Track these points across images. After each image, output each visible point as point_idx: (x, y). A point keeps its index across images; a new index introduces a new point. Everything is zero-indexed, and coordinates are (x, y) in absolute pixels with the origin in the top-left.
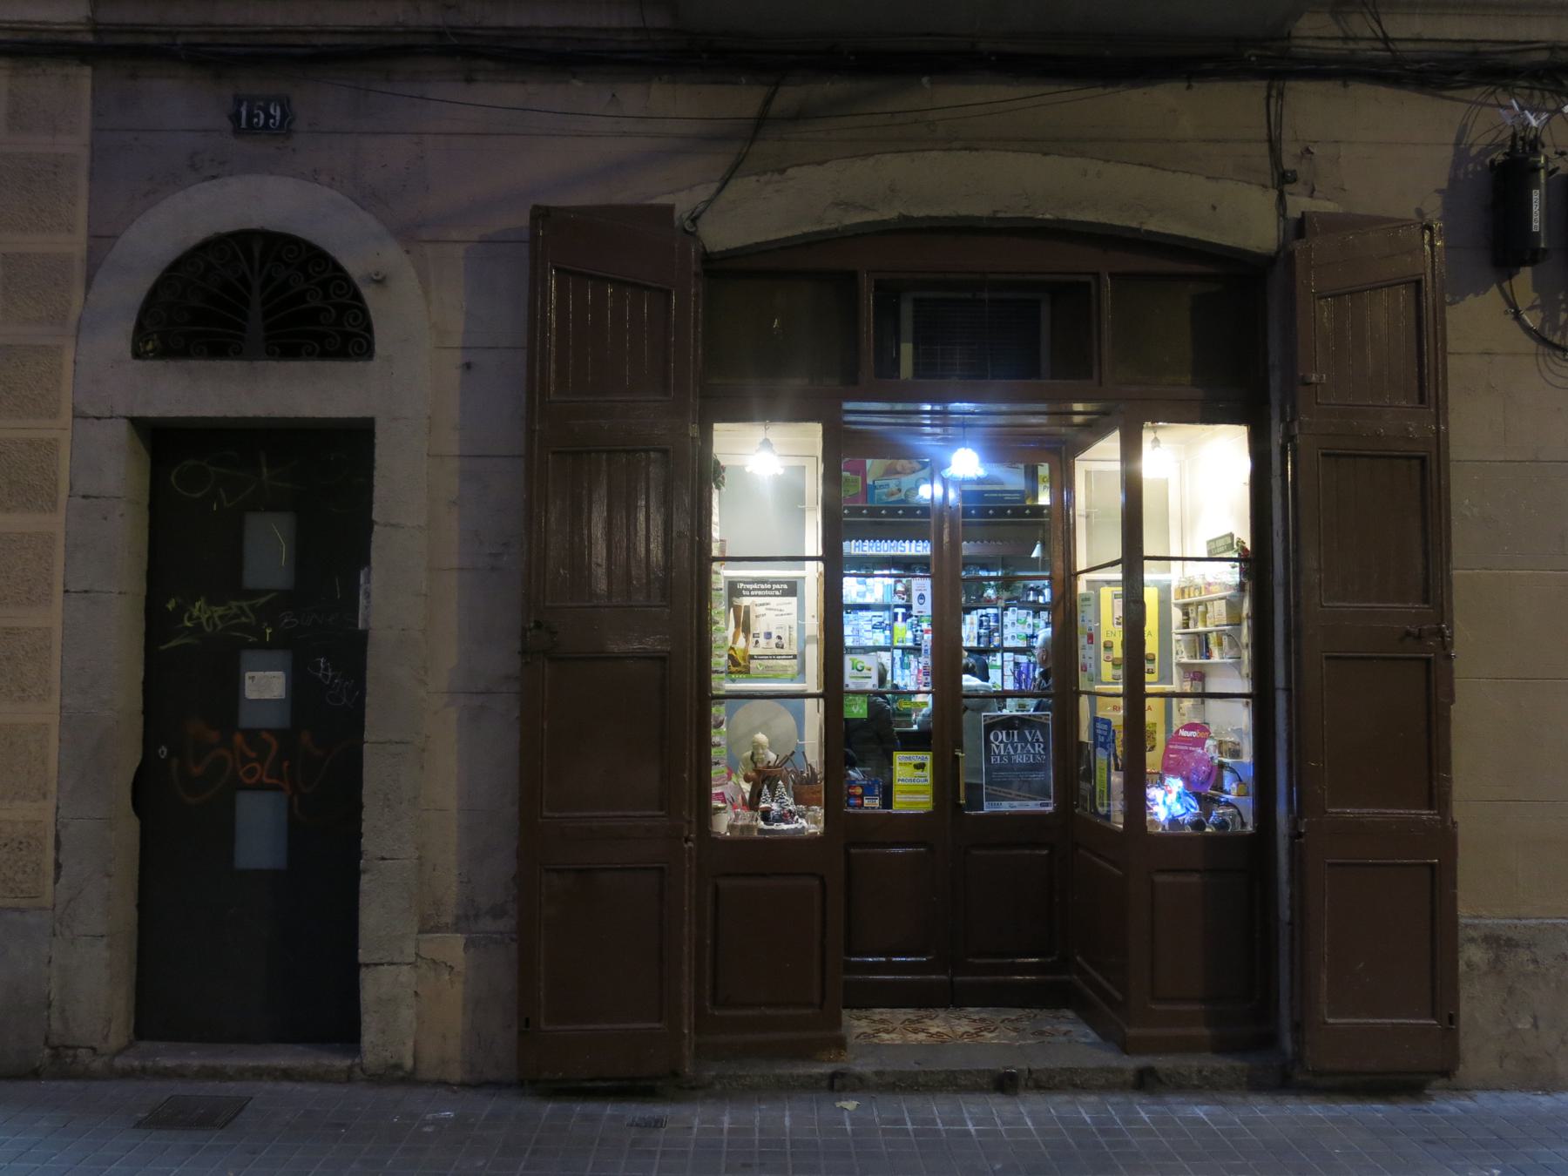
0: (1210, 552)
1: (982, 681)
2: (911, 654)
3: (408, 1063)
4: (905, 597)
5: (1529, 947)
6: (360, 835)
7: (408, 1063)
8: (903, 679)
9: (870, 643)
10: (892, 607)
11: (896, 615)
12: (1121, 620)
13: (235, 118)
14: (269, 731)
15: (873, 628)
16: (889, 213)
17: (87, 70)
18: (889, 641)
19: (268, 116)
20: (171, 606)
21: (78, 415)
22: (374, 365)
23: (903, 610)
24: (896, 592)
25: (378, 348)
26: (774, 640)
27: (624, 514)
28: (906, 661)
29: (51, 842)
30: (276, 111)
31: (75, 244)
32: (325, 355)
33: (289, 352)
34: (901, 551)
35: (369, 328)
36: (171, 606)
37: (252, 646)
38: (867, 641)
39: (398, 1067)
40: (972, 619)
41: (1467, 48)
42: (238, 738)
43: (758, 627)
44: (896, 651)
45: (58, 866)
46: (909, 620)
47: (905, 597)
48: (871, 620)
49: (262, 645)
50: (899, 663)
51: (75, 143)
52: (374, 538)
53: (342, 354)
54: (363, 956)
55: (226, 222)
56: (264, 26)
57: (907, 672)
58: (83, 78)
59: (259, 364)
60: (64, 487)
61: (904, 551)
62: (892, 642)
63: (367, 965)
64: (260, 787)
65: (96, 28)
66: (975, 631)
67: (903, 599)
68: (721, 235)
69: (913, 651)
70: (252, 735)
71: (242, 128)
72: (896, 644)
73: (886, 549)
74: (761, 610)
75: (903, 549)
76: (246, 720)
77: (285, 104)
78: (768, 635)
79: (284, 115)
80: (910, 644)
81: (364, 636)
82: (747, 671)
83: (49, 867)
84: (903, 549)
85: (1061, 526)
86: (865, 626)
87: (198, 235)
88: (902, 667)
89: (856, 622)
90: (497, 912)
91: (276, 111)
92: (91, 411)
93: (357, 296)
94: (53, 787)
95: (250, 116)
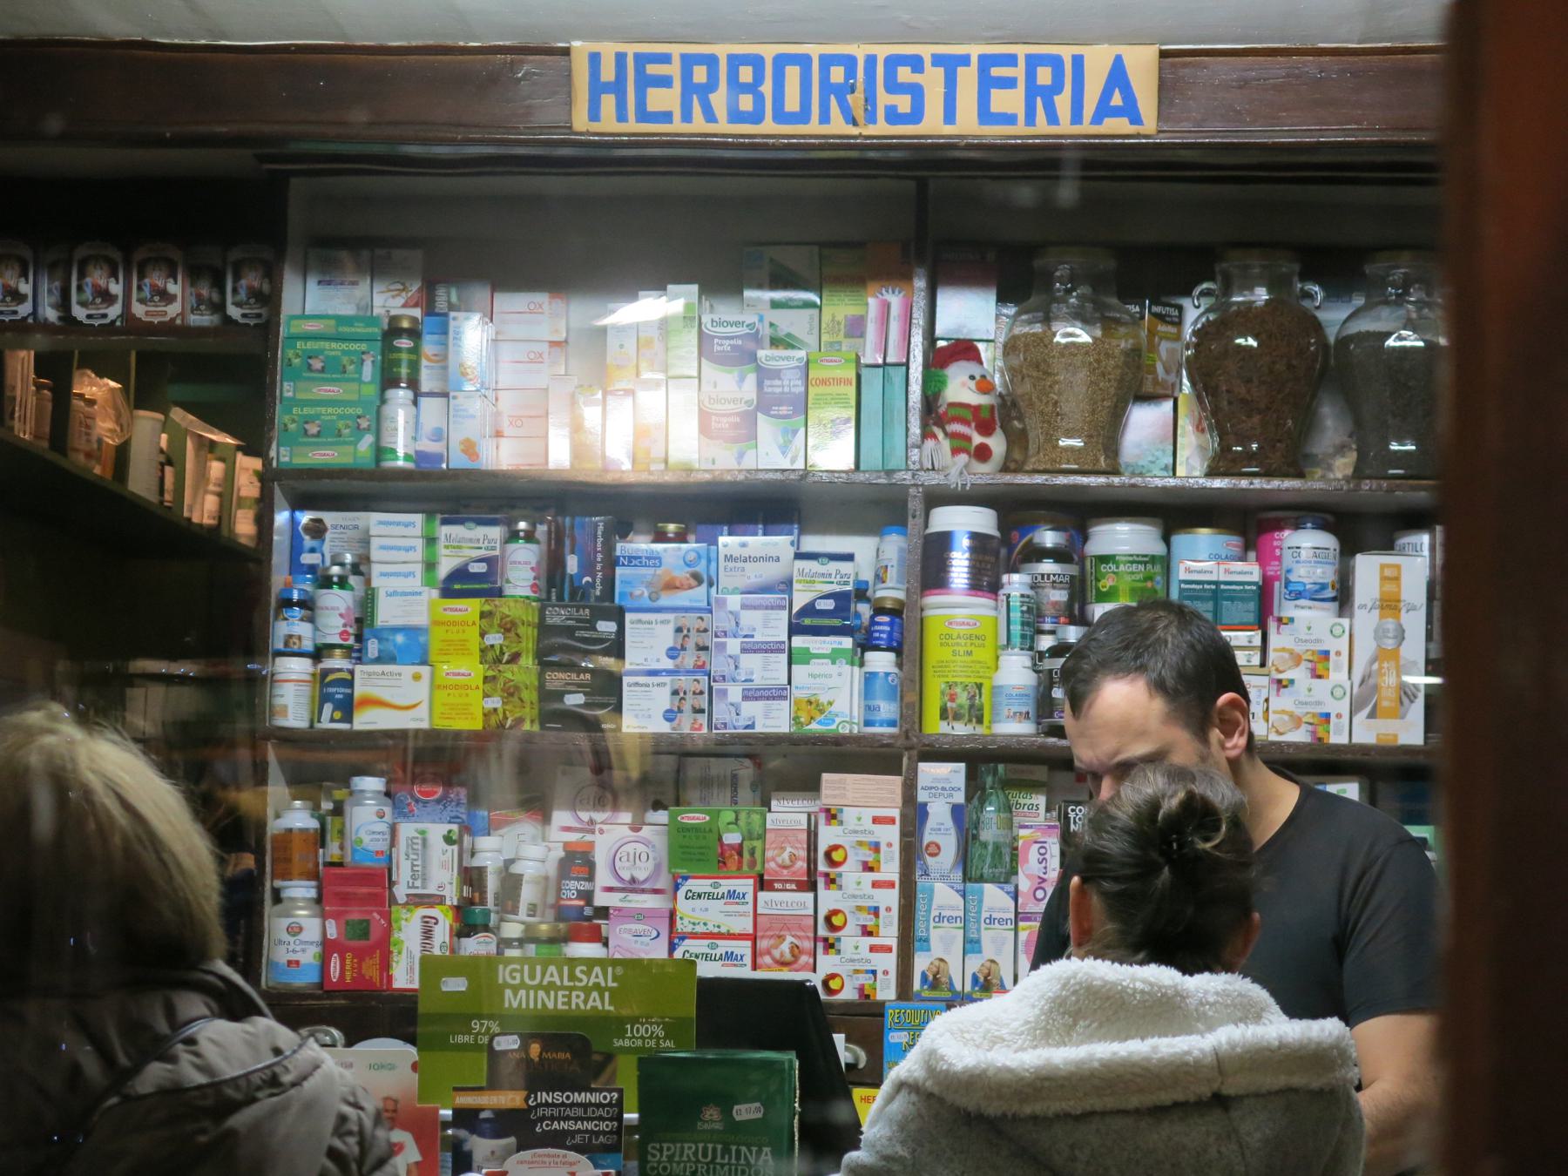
1: (1294, 1010)
2: (1032, 786)
4: (997, 443)
8: (971, 945)
9: (774, 720)
10: (915, 505)
11: (938, 546)
12: (917, 944)
15: (794, 629)
18: (887, 709)
23: (981, 520)
24: (933, 412)
27: (1332, 362)
28: (990, 833)
34: (893, 116)
38: (752, 709)
40: (1391, 578)
44: (930, 772)
46: (1016, 583)
47: (997, 443)
48: (787, 585)
50: (949, 844)
57: (994, 897)
61: (916, 115)
62: (912, 712)
66: (958, 680)
67: (983, 453)
69: (1041, 773)
72: (935, 726)
73: (792, 103)
75: (904, 103)
80: (1015, 727)
84: (904, 103)
86: (750, 619)
88: (970, 870)
89: (698, 594)
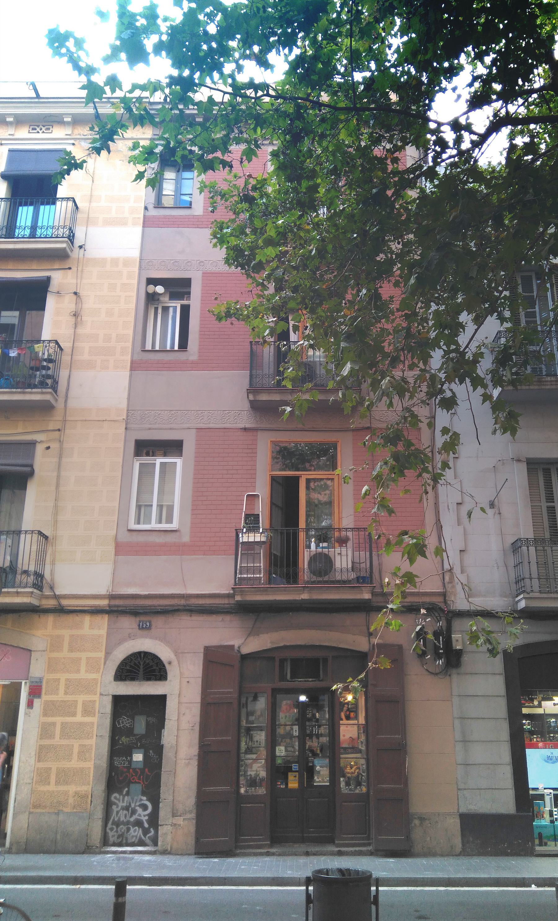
0: (175, 202)
3: (169, 849)
5: (429, 820)
6: (160, 793)
7: (169, 849)
13: (139, 625)
14: (139, 769)
16: (282, 644)
17: (107, 615)
19: (146, 625)
20: (117, 738)
21: (101, 694)
22: (167, 682)
25: (168, 678)
26: (259, 743)
29: (90, 796)
30: (148, 624)
31: (102, 655)
32: (156, 680)
33: (149, 679)
35: (166, 673)
36: (117, 738)
37: (135, 748)
39: (167, 850)
41: (409, 604)
42: (131, 770)
43: (255, 739)
45: (91, 802)
49: (137, 748)
51: (103, 632)
52: (166, 723)
53: (160, 679)
54: (160, 823)
55: (137, 650)
56: (53, 563)
58: (106, 617)
59: (142, 682)
60: (97, 711)
63: (161, 825)
64: (136, 782)
65: (109, 606)
68: (246, 650)
70: (134, 770)
71: (141, 628)
74: (255, 735)
76: (133, 766)
77: (150, 622)
78: (257, 741)
79: (150, 624)
81: (163, 745)
82: (252, 751)
83: (89, 802)
85: (137, 857)
87: (130, 652)
90: (190, 812)
91: (148, 624)
92: (104, 694)
93: (164, 666)
94: (91, 782)
95: (142, 625)
